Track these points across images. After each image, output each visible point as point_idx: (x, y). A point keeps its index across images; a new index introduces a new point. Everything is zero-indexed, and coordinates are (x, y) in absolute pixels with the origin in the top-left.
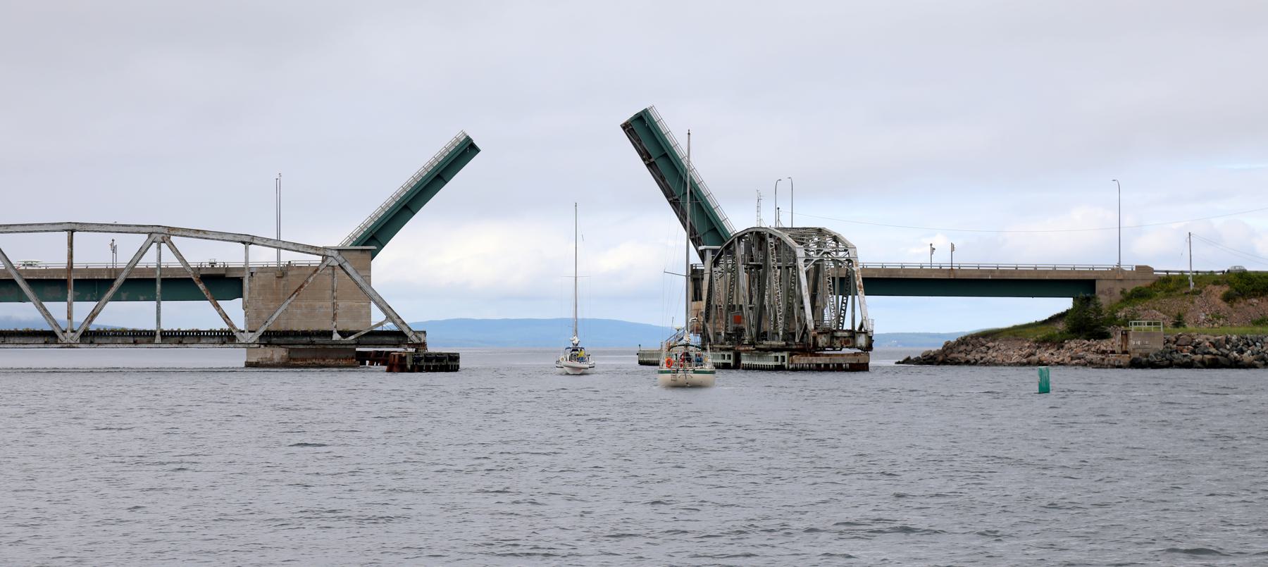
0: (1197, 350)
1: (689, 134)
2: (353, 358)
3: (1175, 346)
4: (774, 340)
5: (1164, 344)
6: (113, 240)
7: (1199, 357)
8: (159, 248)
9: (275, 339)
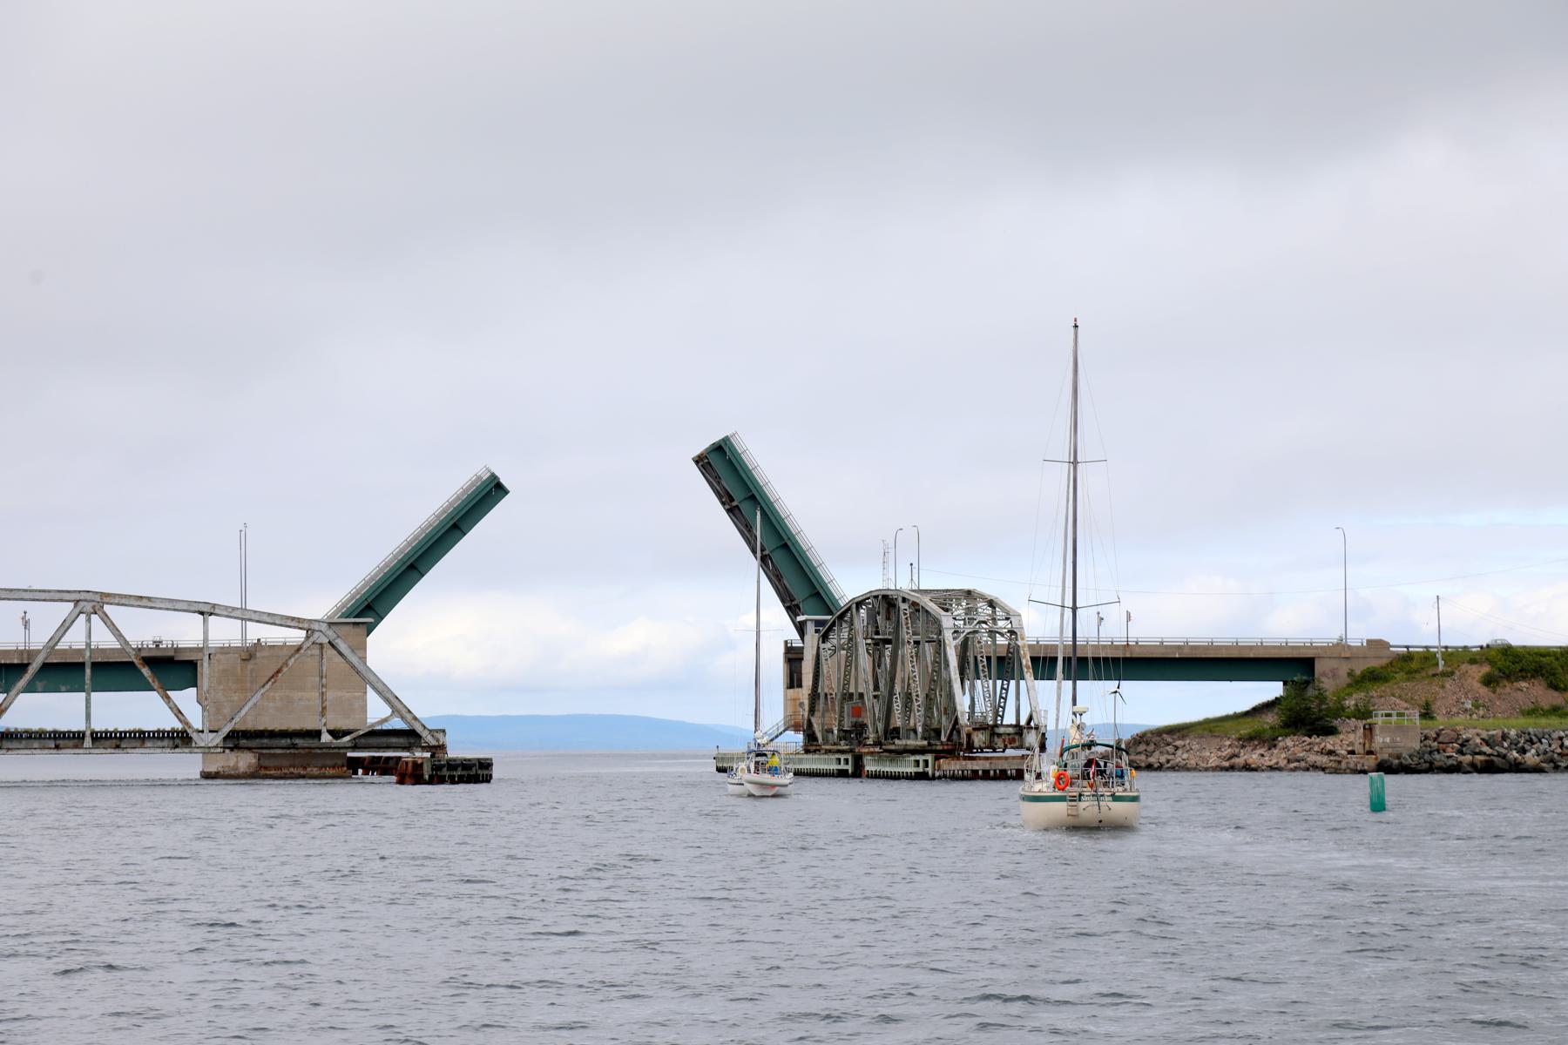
0: (1464, 749)
1: (1076, 326)
2: (343, 766)
3: (1436, 744)
4: (908, 738)
5: (1421, 741)
6: (25, 613)
7: (1468, 758)
8: (89, 620)
9: (244, 741)
